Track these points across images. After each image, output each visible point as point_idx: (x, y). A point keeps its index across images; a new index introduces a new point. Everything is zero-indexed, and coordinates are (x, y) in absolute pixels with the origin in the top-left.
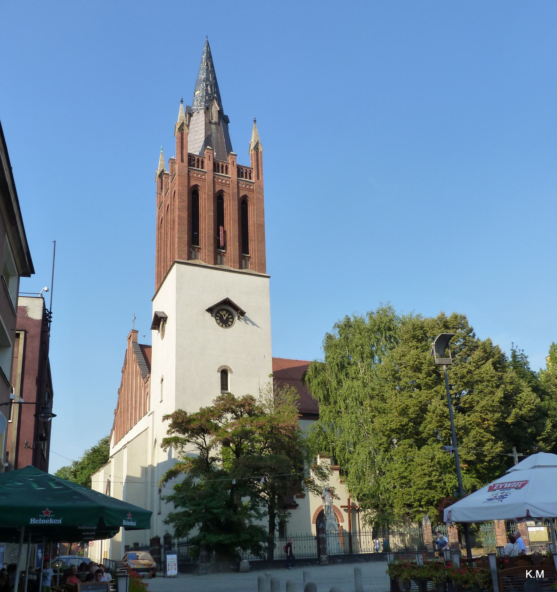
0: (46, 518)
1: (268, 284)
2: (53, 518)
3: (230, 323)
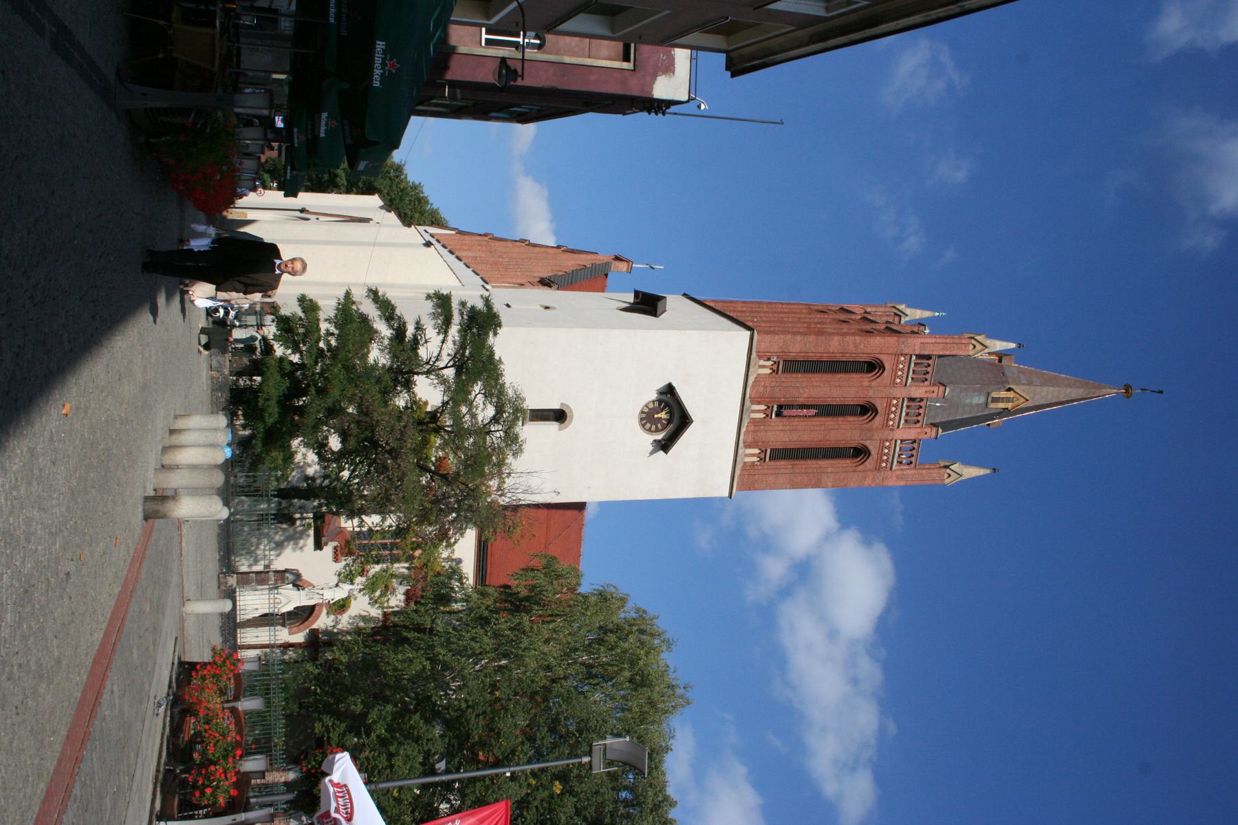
0: (383, 65)
1: (717, 494)
2: (382, 76)
3: (648, 425)
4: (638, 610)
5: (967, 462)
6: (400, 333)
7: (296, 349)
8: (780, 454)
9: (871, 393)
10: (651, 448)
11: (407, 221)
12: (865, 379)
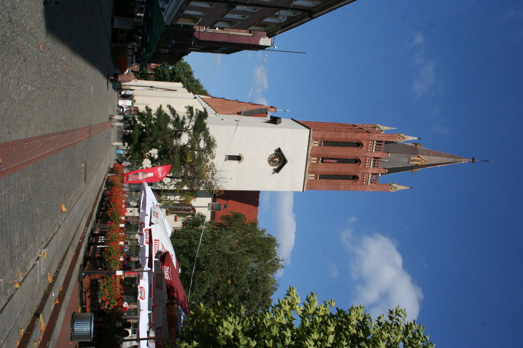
1: (298, 190)
3: (271, 163)
4: (269, 235)
5: (399, 184)
6: (177, 119)
7: (144, 123)
8: (324, 177)
9: (358, 155)
10: (272, 172)
11: (190, 90)
12: (356, 149)
